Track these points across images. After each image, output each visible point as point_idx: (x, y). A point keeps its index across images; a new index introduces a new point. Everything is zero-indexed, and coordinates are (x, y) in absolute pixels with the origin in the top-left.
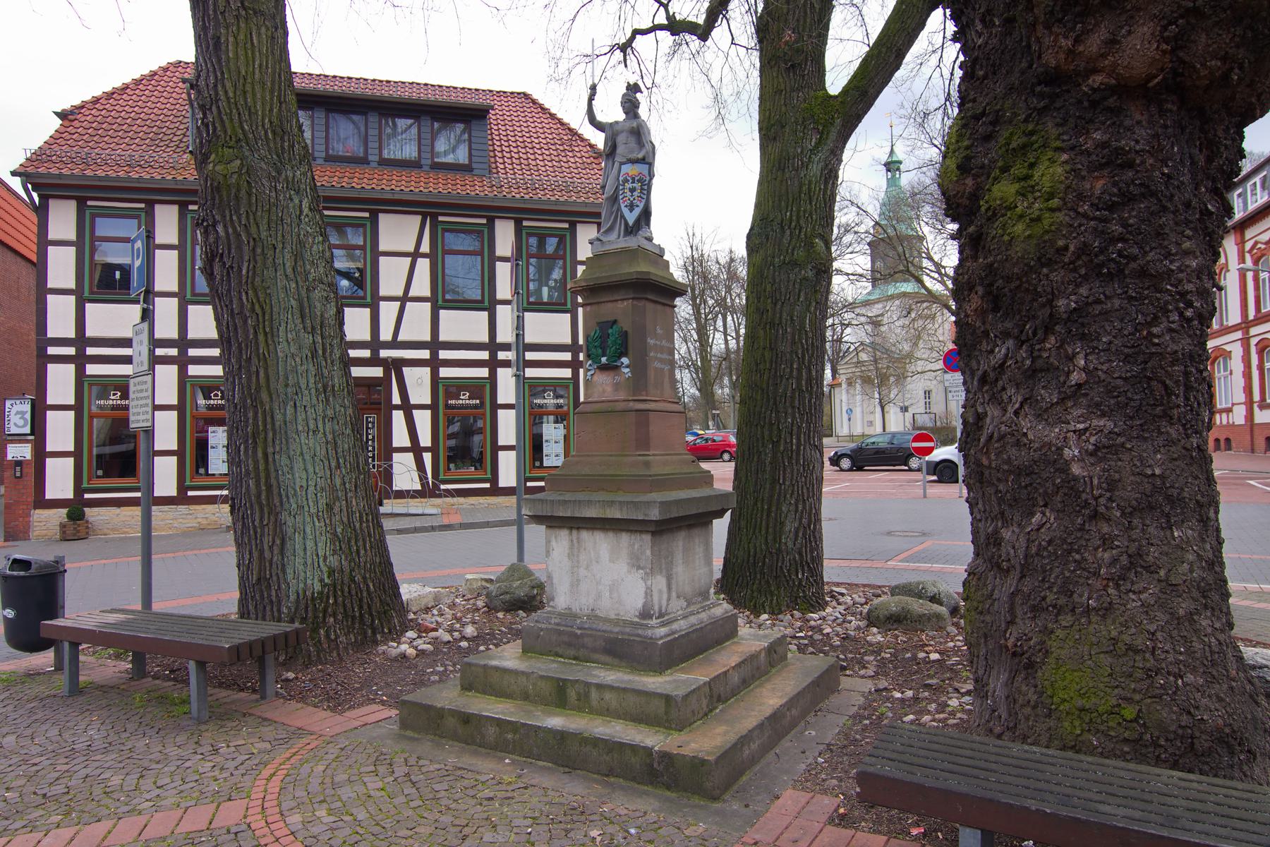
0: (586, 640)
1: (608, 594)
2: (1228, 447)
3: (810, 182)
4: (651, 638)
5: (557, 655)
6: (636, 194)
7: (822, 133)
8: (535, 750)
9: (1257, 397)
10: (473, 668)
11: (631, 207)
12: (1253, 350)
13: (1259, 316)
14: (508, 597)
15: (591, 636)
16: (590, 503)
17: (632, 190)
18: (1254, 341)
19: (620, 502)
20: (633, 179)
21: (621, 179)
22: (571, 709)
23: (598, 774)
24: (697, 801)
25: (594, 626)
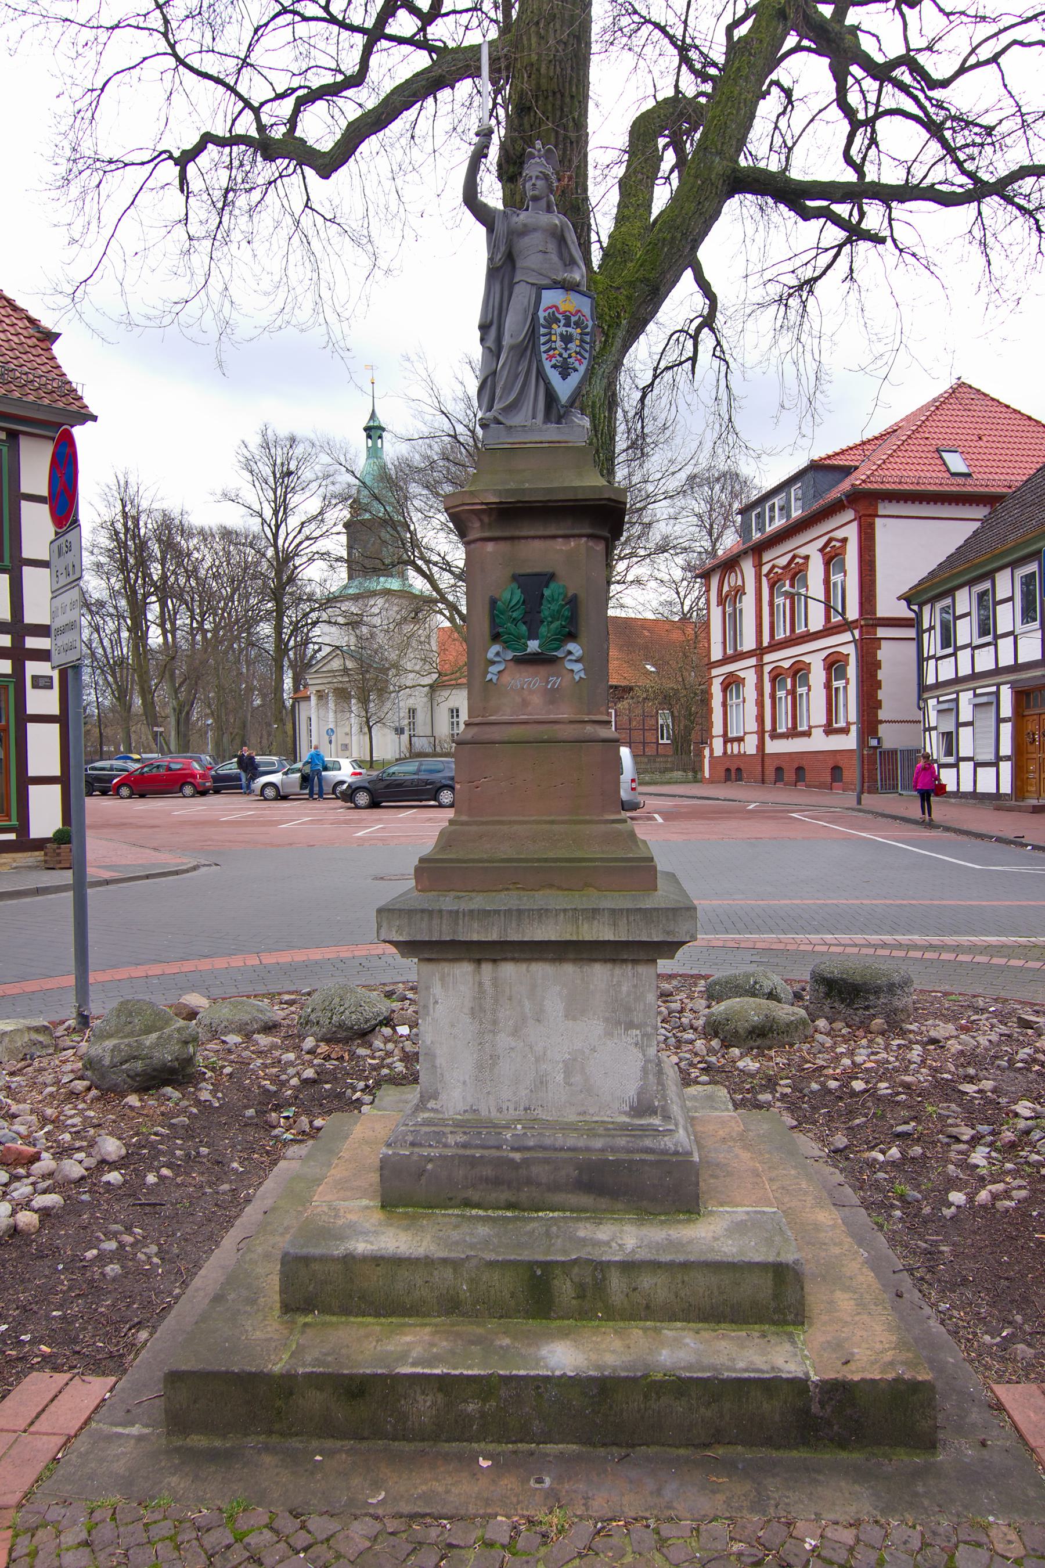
0: (535, 1170)
1: (560, 1078)
2: (739, 778)
3: (594, 403)
4: (676, 1153)
5: (468, 1204)
6: (573, 346)
7: (607, 335)
8: (536, 1426)
9: (768, 726)
10: (315, 1266)
11: (565, 371)
12: (766, 678)
13: (773, 643)
14: (139, 1065)
15: (546, 1161)
16: (542, 914)
17: (567, 339)
18: (767, 669)
19: (613, 911)
20: (568, 319)
21: (542, 314)
22: (562, 1318)
23: (687, 1446)
24: (905, 1458)
25: (548, 1142)
